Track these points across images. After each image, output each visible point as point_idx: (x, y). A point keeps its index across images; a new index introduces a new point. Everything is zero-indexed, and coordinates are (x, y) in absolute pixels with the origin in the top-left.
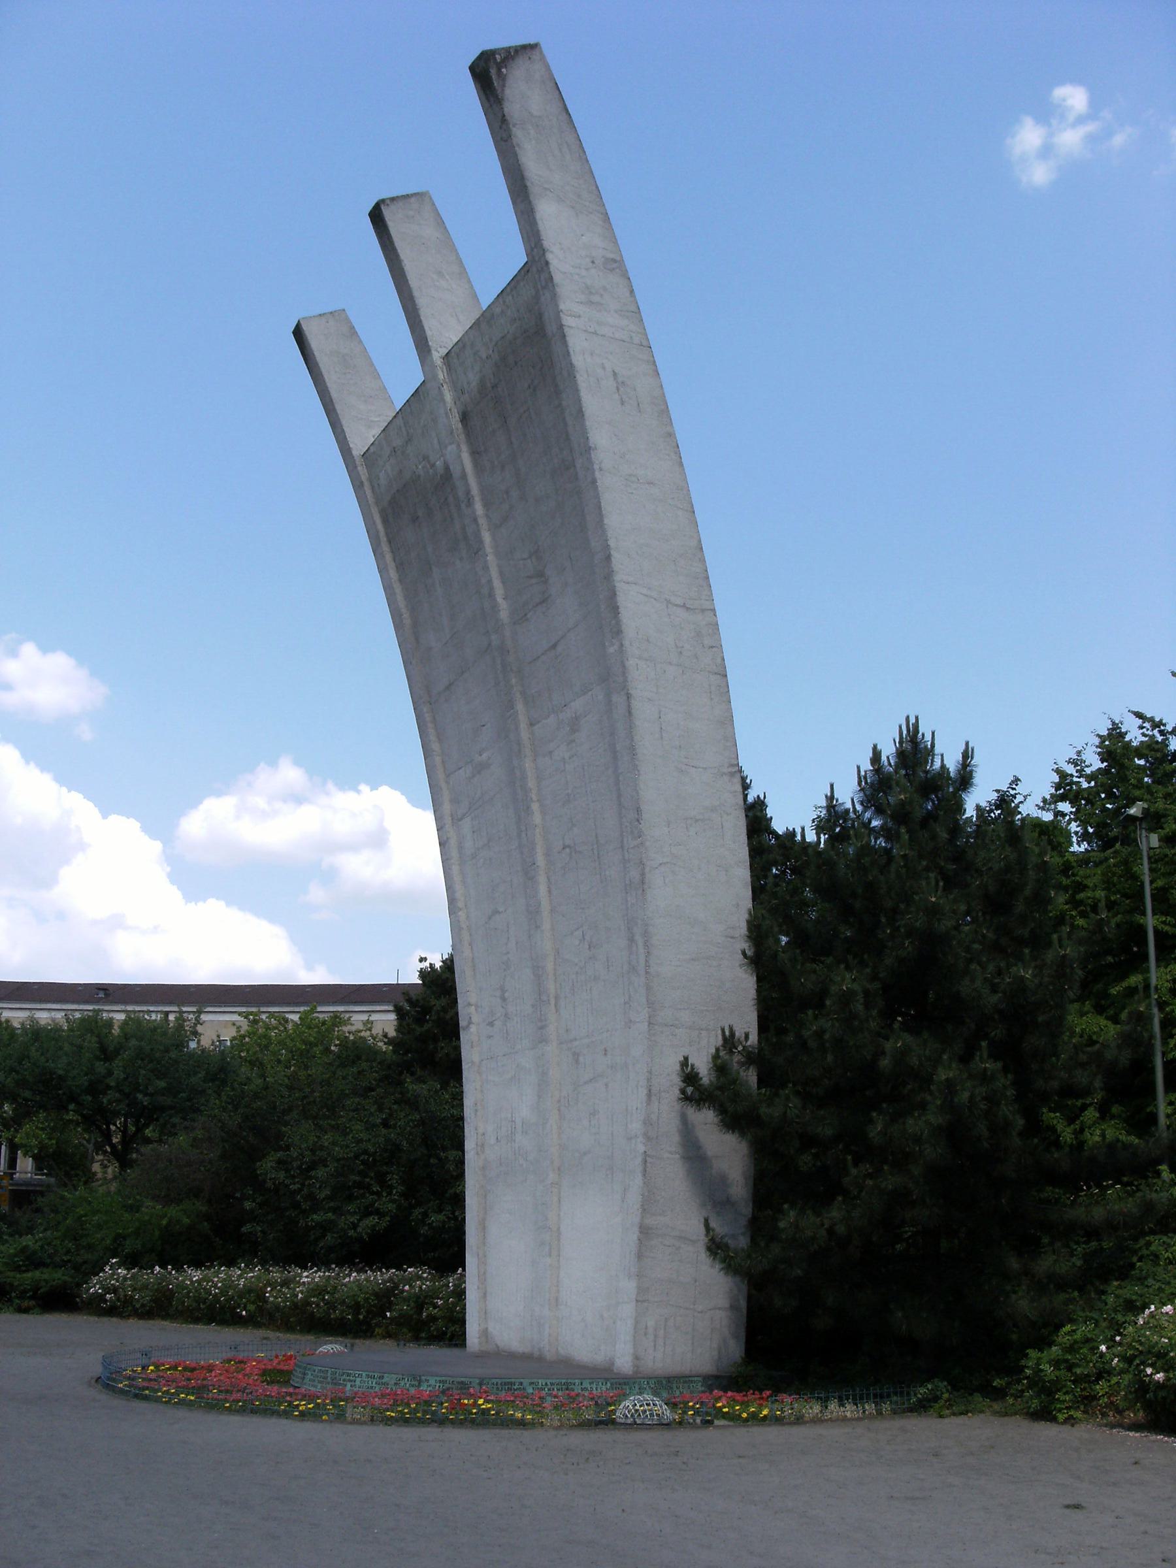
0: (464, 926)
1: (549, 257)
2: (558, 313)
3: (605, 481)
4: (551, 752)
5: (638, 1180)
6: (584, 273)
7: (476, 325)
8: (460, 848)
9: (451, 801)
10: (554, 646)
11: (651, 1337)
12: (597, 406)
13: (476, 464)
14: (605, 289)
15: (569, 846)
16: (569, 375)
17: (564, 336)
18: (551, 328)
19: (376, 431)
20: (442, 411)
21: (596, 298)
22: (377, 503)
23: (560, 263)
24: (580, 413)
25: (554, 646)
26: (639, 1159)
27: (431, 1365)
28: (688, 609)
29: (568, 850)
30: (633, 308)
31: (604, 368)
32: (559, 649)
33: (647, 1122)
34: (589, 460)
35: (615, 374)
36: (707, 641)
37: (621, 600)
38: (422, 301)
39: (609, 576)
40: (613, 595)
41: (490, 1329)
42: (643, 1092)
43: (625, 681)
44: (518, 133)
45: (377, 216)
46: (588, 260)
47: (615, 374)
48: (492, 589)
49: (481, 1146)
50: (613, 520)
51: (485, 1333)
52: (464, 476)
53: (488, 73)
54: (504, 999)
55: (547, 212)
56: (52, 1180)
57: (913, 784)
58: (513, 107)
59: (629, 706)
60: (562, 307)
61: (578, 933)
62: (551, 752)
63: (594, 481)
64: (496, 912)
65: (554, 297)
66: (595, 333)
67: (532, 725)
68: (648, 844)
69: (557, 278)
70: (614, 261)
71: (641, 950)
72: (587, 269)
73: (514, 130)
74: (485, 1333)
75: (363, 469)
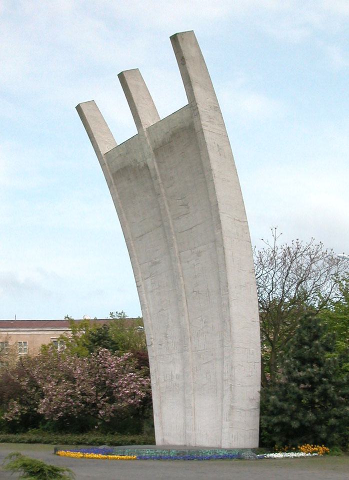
0: (148, 313)
1: (198, 106)
2: (201, 125)
3: (216, 180)
4: (188, 262)
6: (208, 111)
8: (146, 288)
9: (142, 273)
11: (234, 438)
12: (213, 155)
13: (159, 166)
14: (215, 117)
15: (196, 291)
16: (204, 145)
17: (203, 133)
18: (197, 129)
20: (146, 147)
21: (212, 120)
22: (111, 171)
23: (202, 108)
24: (208, 158)
27: (147, 450)
28: (240, 221)
30: (222, 123)
31: (214, 143)
32: (193, 230)
34: (211, 173)
35: (218, 146)
36: (246, 231)
37: (221, 218)
38: (138, 108)
39: (217, 210)
40: (219, 216)
41: (165, 439)
43: (223, 244)
46: (210, 107)
47: (218, 146)
48: (165, 207)
49: (157, 383)
50: (218, 193)
52: (154, 169)
55: (197, 90)
56: (40, 422)
59: (224, 251)
60: (202, 123)
61: (200, 318)
62: (188, 262)
63: (212, 180)
66: (212, 132)
67: (179, 252)
68: (230, 293)
69: (201, 113)
70: (217, 107)
71: (228, 323)
72: (209, 110)
73: (187, 62)
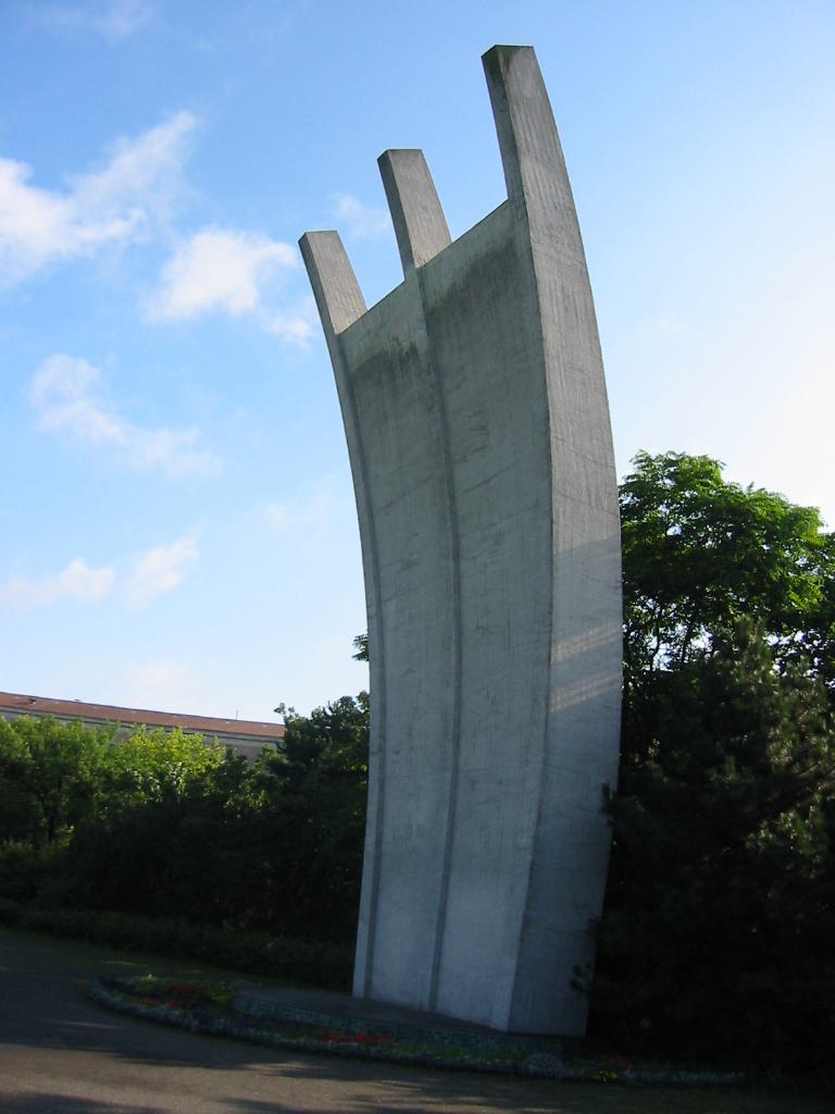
4: (474, 558)
5: (525, 881)
7: (449, 247)
10: (487, 482)
15: (482, 628)
19: (353, 319)
24: (538, 313)
25: (487, 482)
26: (527, 867)
29: (481, 631)
32: (492, 484)
33: (536, 838)
42: (534, 816)
44: (514, 107)
45: (384, 162)
51: (368, 984)
53: (497, 63)
54: (410, 735)
57: (360, 640)
58: (513, 90)
62: (474, 558)
64: (410, 671)
65: (527, 227)
70: (570, 209)
74: (368, 984)
75: (338, 345)
